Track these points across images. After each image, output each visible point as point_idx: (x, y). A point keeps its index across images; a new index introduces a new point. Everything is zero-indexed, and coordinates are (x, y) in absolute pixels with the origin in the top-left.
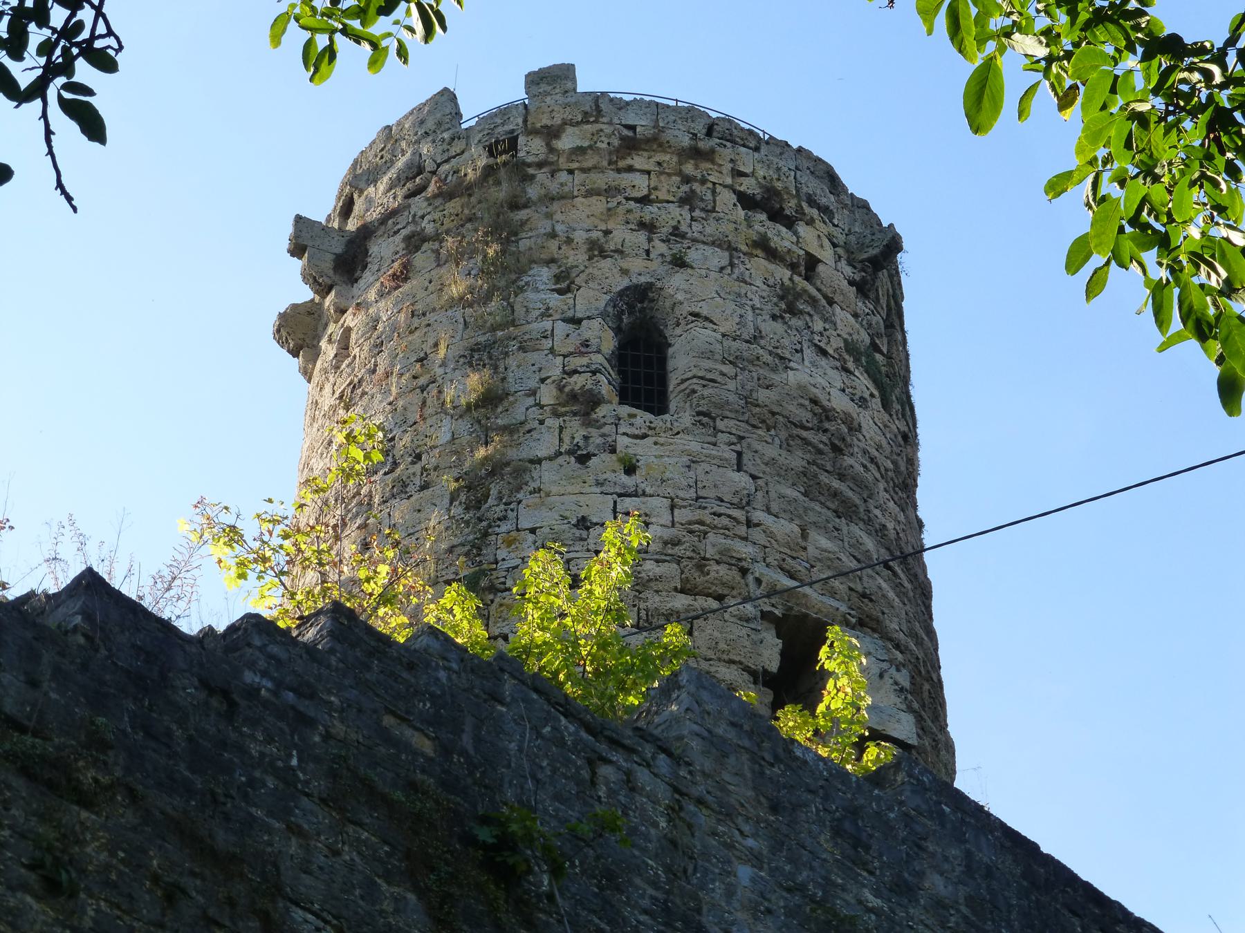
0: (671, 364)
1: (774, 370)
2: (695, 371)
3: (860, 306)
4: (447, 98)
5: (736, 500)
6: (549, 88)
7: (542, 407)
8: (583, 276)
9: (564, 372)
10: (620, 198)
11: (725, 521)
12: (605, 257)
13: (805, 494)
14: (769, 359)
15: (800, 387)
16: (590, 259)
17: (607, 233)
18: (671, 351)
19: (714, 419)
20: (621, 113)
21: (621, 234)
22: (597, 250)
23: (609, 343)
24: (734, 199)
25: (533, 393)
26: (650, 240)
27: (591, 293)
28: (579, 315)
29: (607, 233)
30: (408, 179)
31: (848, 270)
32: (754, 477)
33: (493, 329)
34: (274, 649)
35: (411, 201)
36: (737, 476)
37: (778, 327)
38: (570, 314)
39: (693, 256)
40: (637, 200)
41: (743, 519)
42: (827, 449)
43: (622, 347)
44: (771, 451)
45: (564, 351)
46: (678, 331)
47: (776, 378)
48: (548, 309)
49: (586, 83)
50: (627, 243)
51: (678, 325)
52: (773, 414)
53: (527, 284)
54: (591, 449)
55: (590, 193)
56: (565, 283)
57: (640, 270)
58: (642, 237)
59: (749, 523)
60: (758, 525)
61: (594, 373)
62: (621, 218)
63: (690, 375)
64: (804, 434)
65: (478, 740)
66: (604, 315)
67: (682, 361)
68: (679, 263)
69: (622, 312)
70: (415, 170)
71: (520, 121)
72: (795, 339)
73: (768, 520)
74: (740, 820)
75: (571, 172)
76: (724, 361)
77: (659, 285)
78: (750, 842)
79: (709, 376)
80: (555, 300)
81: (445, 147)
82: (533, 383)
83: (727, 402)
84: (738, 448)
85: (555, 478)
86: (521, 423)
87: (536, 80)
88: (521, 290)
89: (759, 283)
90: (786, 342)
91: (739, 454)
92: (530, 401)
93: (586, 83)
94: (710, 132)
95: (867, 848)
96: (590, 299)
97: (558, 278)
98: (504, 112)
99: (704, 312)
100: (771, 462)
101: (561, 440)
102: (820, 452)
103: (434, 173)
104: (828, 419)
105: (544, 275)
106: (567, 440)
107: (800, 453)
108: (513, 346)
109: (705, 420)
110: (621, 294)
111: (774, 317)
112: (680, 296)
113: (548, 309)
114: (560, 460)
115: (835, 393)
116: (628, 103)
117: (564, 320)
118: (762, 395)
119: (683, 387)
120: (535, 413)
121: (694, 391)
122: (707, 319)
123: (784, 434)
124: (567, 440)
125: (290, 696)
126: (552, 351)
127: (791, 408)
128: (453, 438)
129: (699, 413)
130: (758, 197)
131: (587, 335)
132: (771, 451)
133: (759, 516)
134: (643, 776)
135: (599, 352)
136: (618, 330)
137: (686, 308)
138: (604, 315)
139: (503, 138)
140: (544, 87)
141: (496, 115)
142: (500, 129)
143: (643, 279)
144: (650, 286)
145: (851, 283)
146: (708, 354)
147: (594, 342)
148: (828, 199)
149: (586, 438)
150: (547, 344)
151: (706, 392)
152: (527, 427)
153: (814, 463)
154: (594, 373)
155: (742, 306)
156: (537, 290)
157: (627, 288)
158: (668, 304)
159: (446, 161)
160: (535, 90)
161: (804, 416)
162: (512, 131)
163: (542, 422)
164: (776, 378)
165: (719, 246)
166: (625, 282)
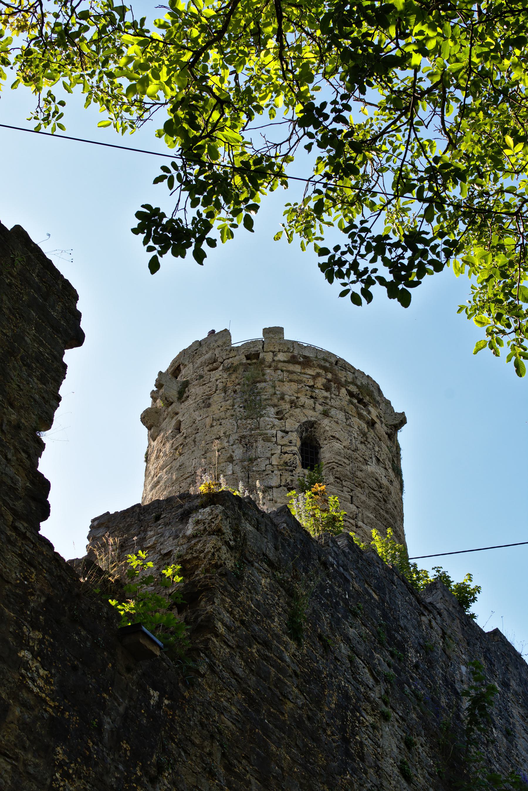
0: (322, 455)
1: (363, 464)
2: (334, 460)
3: (389, 443)
4: (226, 333)
5: (351, 516)
6: (273, 336)
7: (273, 465)
8: (288, 414)
9: (281, 452)
10: (303, 385)
11: (348, 524)
12: (297, 408)
13: (376, 517)
14: (361, 459)
15: (372, 473)
16: (291, 407)
17: (297, 398)
18: (322, 450)
19: (341, 481)
20: (303, 350)
21: (303, 399)
22: (293, 404)
23: (299, 443)
24: (346, 392)
25: (269, 458)
26: (315, 403)
27: (292, 421)
28: (287, 430)
29: (298, 398)
30: (209, 364)
31: (385, 428)
32: (358, 507)
33: (251, 429)
34: (335, 549)
35: (211, 373)
36: (351, 506)
37: (363, 446)
38: (283, 429)
39: (333, 412)
40: (309, 387)
41: (354, 524)
42: (382, 500)
43: (302, 445)
44: (363, 498)
45: (281, 443)
46: (325, 442)
47: (364, 467)
48: (274, 425)
49: (288, 336)
50: (306, 404)
51: (325, 440)
52: (363, 482)
53: (265, 413)
54: (294, 486)
55: (291, 381)
56: (280, 415)
57: (311, 415)
58: (312, 401)
59: (357, 526)
60: (360, 527)
61: (294, 454)
62: (304, 393)
63: (332, 461)
64: (374, 492)
65: (390, 599)
66: (297, 431)
67: (327, 454)
68: (326, 414)
69: (303, 431)
70: (213, 360)
71: (261, 347)
72: (370, 453)
73: (364, 526)
74: (461, 647)
75: (282, 371)
76: (345, 457)
77: (319, 422)
78: (464, 656)
79: (339, 463)
80: (276, 422)
81: (228, 353)
82: (269, 455)
83: (347, 475)
84: (351, 494)
85: (279, 496)
86: (264, 471)
87: (267, 331)
88: (262, 416)
89: (356, 428)
90: (367, 453)
91: (352, 497)
92: (267, 462)
93: (288, 336)
94: (337, 363)
95: (494, 666)
96: (291, 424)
97: (277, 413)
98: (254, 343)
99: (337, 436)
100: (363, 502)
101: (281, 480)
102: (380, 501)
103: (222, 363)
104: (381, 488)
105: (272, 411)
106: (284, 481)
107: (373, 500)
108: (260, 439)
109: (338, 480)
110: (304, 423)
111: (362, 443)
112: (327, 428)
113: (274, 425)
114: (281, 488)
115: (383, 477)
116: (305, 347)
117: (281, 431)
118: (359, 474)
119: (328, 465)
120: (269, 467)
121: (334, 468)
122: (338, 439)
123: (367, 491)
124: (284, 481)
125: (341, 569)
126: (276, 443)
127: (370, 481)
128: (233, 473)
129: (336, 478)
130: (355, 393)
131: (291, 438)
132: (363, 498)
133: (360, 524)
134: (434, 623)
135: (296, 446)
136: (301, 438)
137: (330, 434)
138: (297, 431)
139: (252, 354)
140: (271, 335)
141: (250, 343)
142: (252, 349)
143: (313, 419)
144: (315, 422)
145: (387, 433)
146: (339, 454)
147: (294, 441)
148: (378, 398)
149: (292, 481)
150: (274, 439)
151: (339, 469)
152: (266, 473)
153: (378, 505)
154: (294, 454)
155: (351, 436)
156: (269, 417)
157: (306, 422)
158: (322, 431)
159: (228, 359)
160: (267, 335)
161: (374, 485)
162: (257, 351)
163: (273, 472)
164: (364, 467)
165: (341, 410)
166: (306, 419)
